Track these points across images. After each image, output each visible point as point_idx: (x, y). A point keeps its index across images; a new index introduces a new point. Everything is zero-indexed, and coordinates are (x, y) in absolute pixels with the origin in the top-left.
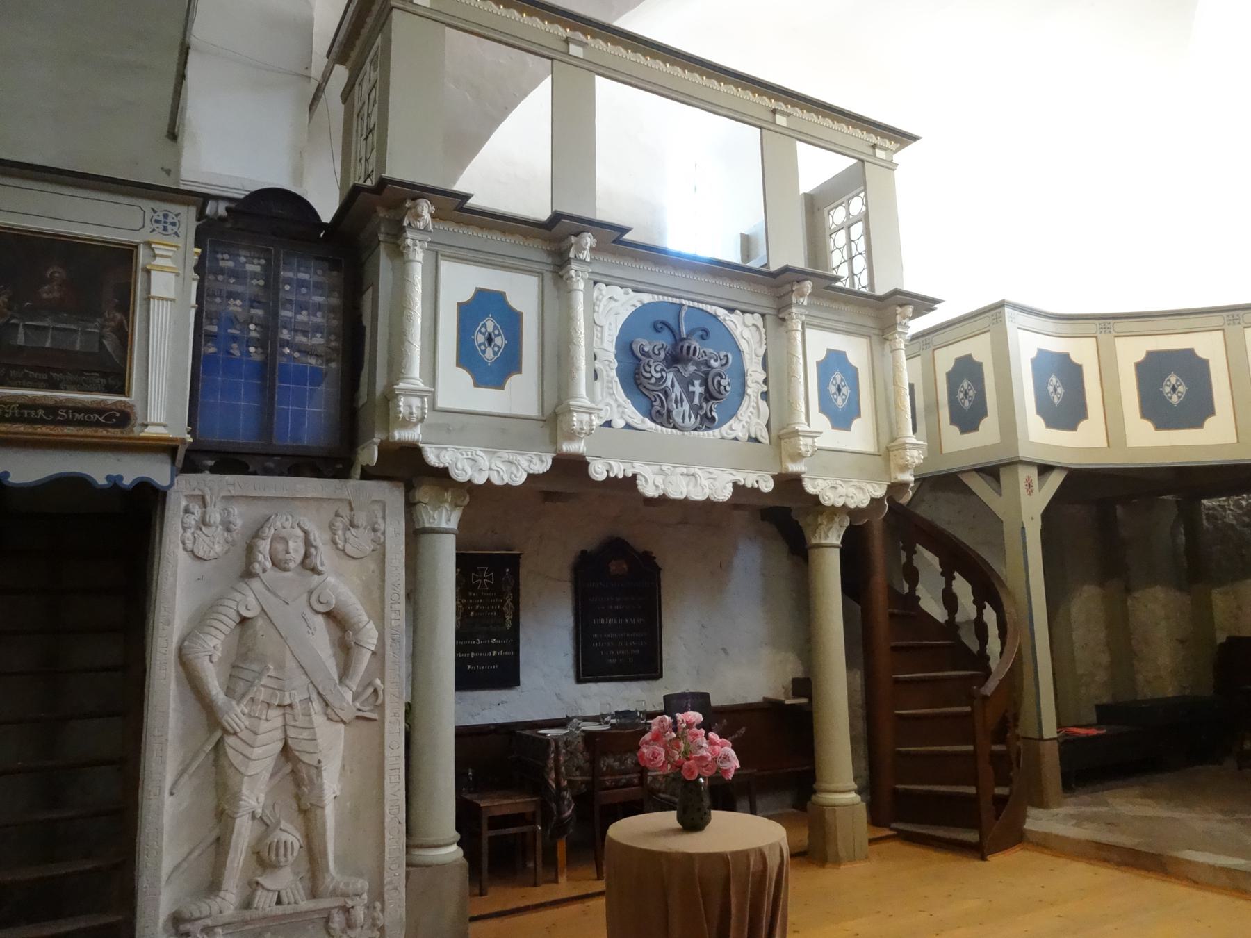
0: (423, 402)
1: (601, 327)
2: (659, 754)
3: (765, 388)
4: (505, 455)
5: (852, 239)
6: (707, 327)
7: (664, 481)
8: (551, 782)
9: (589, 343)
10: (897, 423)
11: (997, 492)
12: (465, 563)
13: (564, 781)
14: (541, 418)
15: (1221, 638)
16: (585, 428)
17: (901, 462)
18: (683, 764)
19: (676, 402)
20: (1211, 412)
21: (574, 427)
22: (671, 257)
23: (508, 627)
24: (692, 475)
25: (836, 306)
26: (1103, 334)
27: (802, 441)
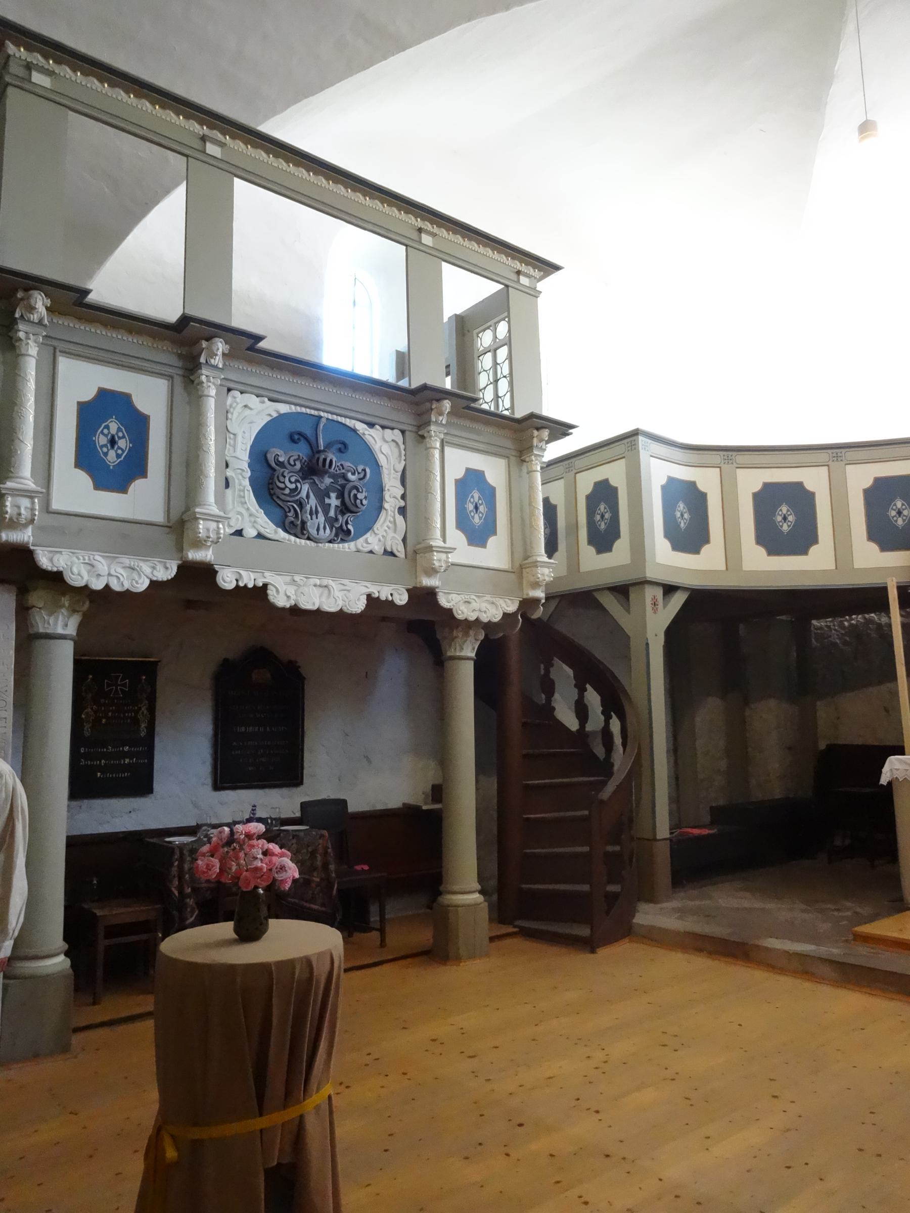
0: (33, 503)
1: (234, 435)
2: (213, 866)
3: (402, 503)
4: (126, 560)
5: (498, 362)
6: (347, 442)
7: (295, 591)
8: (173, 889)
9: (220, 452)
10: (531, 543)
11: (625, 609)
12: (81, 667)
13: (188, 888)
14: (167, 524)
15: (822, 745)
16: (212, 536)
17: (532, 579)
18: (241, 875)
19: (311, 514)
20: (815, 541)
21: (200, 535)
22: (326, 373)
23: (143, 734)
24: (326, 586)
25: (475, 426)
26: (726, 465)
27: (436, 556)
